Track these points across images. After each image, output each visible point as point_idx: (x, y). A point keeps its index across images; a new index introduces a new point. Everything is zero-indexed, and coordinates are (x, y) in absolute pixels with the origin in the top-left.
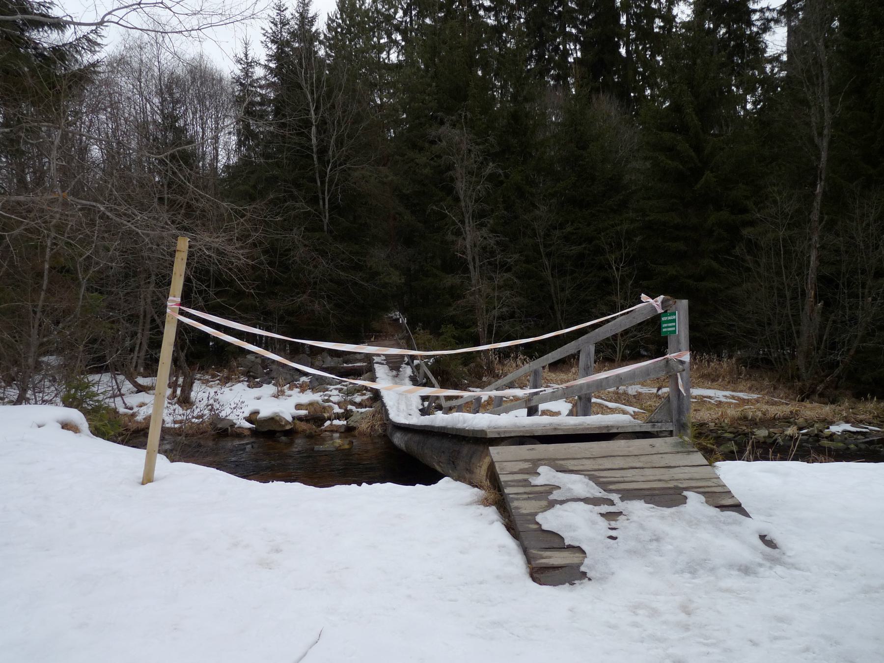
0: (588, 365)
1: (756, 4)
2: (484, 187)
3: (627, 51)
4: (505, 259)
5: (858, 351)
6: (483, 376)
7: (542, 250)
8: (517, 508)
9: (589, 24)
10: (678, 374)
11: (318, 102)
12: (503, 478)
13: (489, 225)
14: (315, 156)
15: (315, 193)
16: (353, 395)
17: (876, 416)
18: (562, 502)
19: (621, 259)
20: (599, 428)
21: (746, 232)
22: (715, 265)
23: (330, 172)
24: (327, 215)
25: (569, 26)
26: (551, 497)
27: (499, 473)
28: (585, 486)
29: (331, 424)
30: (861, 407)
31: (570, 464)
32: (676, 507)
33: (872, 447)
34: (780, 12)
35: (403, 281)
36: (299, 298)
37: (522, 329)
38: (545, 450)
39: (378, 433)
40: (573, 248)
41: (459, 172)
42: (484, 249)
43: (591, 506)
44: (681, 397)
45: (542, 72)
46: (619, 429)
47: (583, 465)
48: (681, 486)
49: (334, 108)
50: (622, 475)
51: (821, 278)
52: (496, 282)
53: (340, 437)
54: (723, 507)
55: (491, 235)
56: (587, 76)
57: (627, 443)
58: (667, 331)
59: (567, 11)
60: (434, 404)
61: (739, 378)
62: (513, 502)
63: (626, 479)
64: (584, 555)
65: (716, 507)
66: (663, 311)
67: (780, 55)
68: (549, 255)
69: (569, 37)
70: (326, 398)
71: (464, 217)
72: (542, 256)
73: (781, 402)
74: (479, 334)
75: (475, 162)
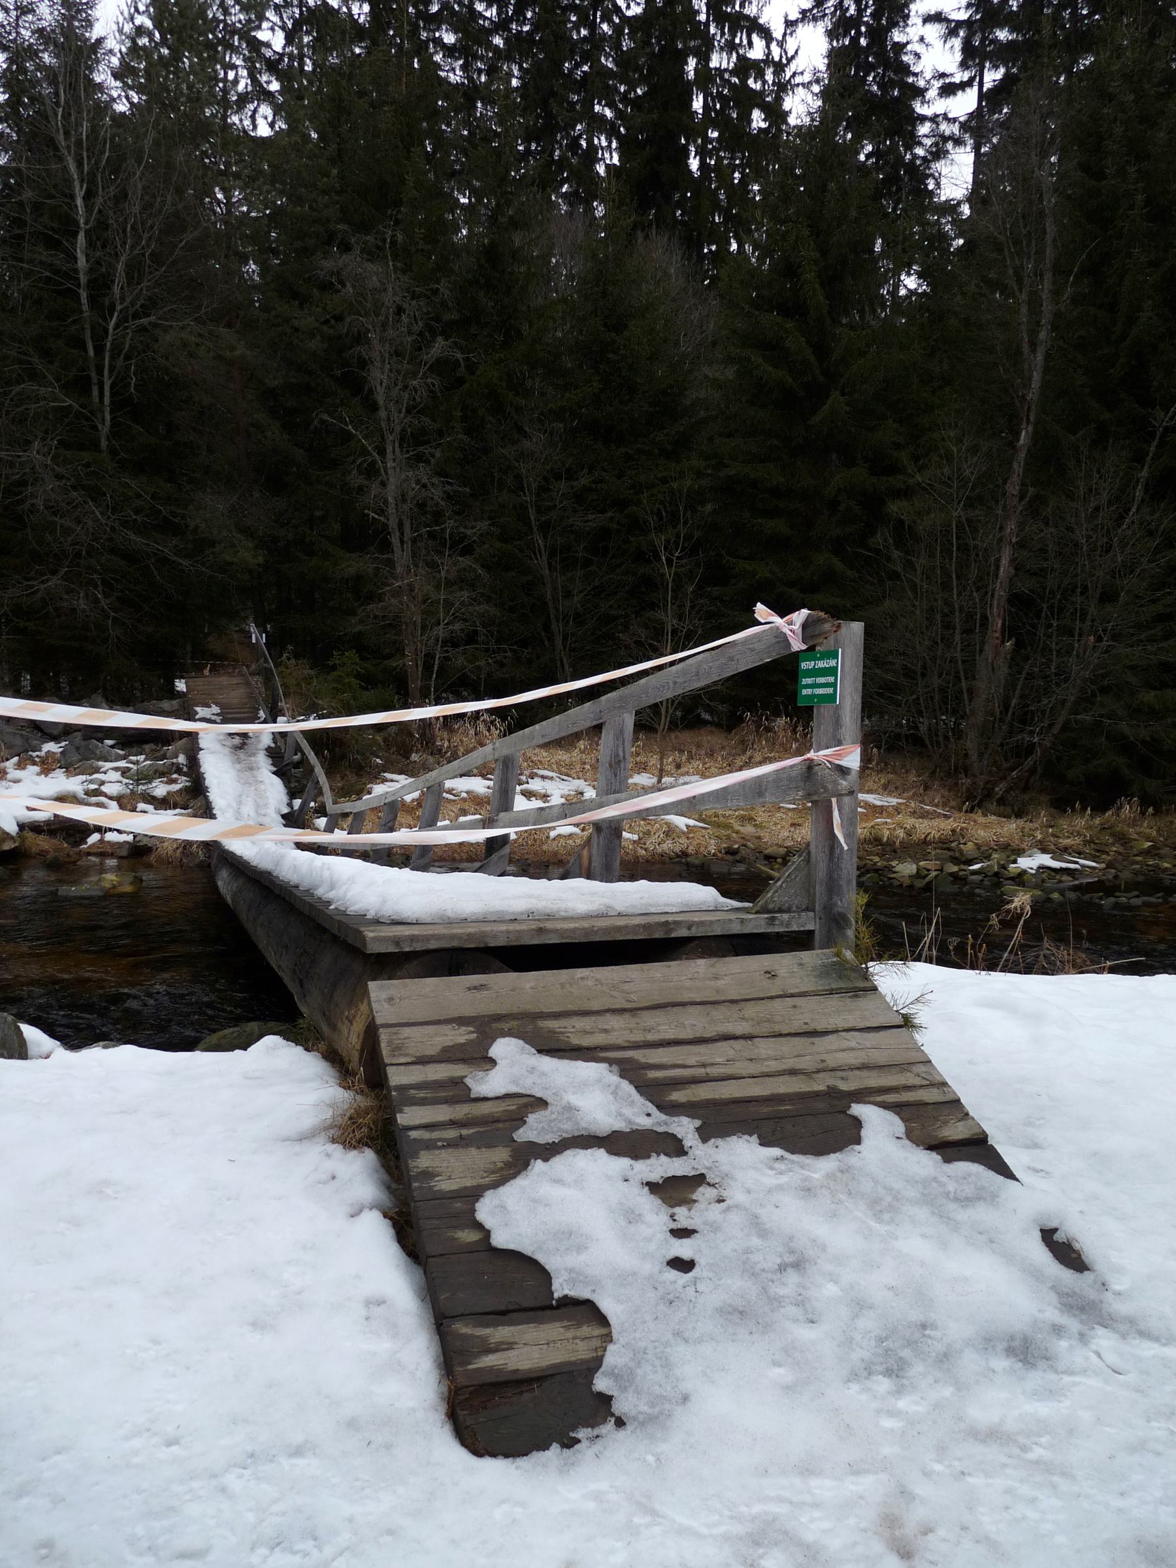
0: (618, 755)
1: (926, 105)
2: (427, 384)
3: (703, 166)
4: (462, 530)
5: (1065, 727)
6: (411, 751)
7: (532, 518)
8: (428, 1175)
9: (637, 103)
10: (834, 800)
11: (92, 181)
12: (397, 1077)
13: (433, 461)
14: (84, 295)
15: (84, 370)
16: (150, 782)
17: (1087, 841)
18: (548, 1151)
19: (677, 544)
20: (647, 927)
21: (895, 507)
22: (838, 565)
23: (115, 329)
24: (108, 417)
25: (599, 103)
26: (523, 1135)
27: (387, 1061)
28: (611, 1097)
29: (101, 841)
30: (1064, 824)
31: (575, 1031)
32: (837, 1154)
33: (1087, 897)
34: (964, 126)
35: (261, 560)
36: (43, 582)
37: (489, 664)
38: (513, 990)
39: (197, 861)
40: (590, 517)
41: (377, 349)
42: (421, 506)
43: (624, 1163)
44: (837, 851)
45: (546, 180)
46: (694, 930)
47: (606, 1031)
48: (844, 1086)
49: (126, 196)
50: (704, 1059)
51: (1015, 599)
52: (443, 574)
53: (119, 868)
54: (949, 1150)
55: (435, 480)
56: (628, 200)
57: (712, 966)
58: (813, 696)
59: (598, 74)
60: (312, 804)
61: (868, 768)
62: (415, 1155)
63: (714, 1071)
64: (604, 1331)
65: (931, 1148)
66: (804, 647)
67: (959, 203)
68: (545, 528)
69: (597, 124)
70: (93, 787)
71: (384, 440)
72: (531, 529)
73: (936, 812)
74: (406, 671)
75: (410, 333)
